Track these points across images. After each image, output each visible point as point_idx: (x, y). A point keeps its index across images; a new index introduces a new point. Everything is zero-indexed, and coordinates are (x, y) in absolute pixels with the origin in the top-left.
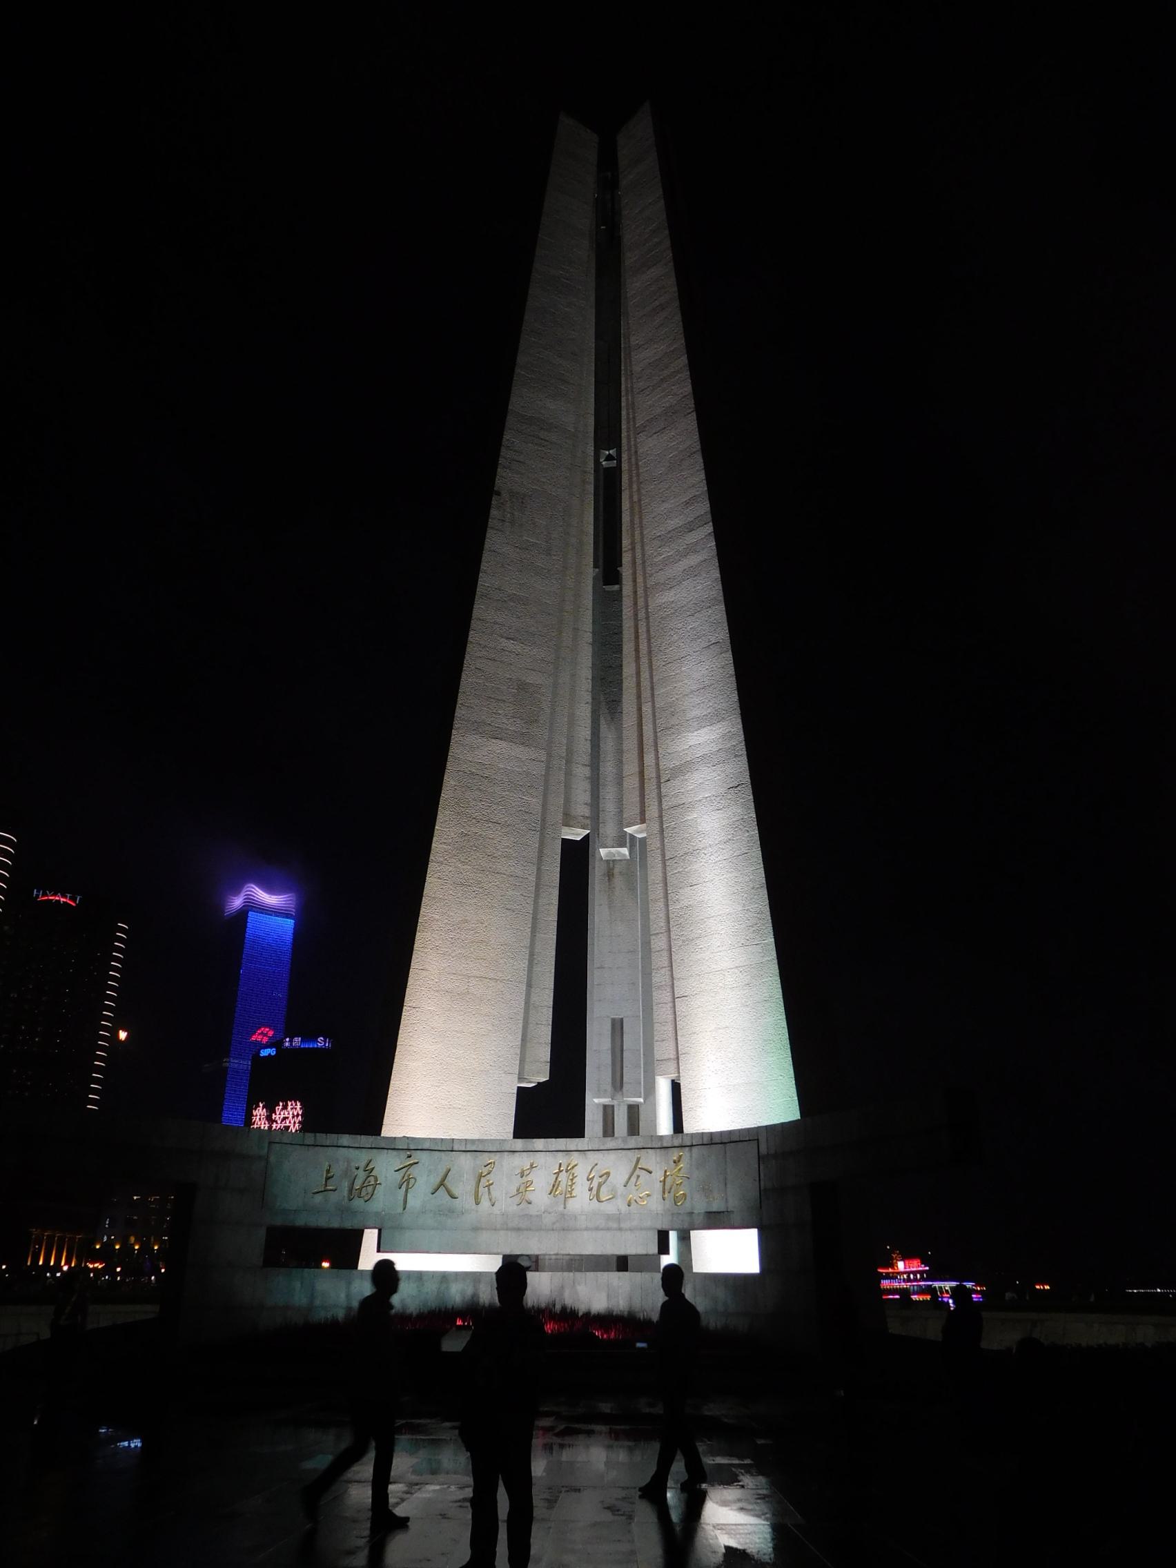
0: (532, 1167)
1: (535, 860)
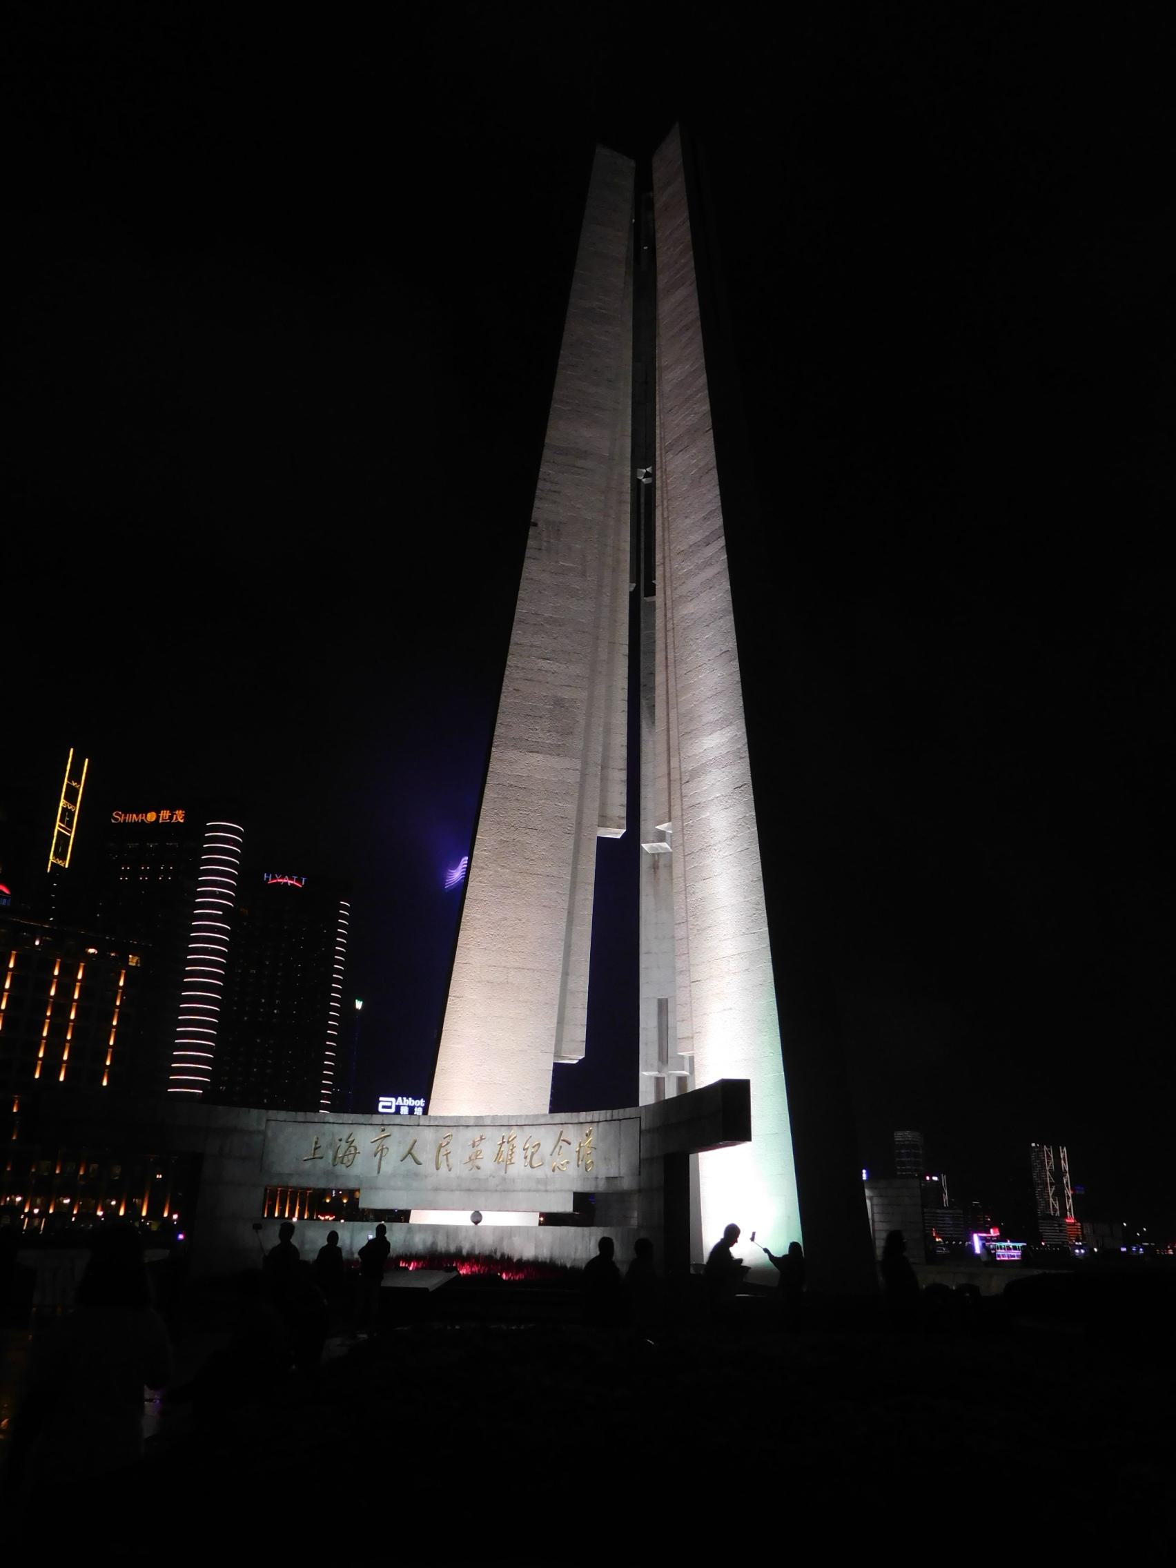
1: (570, 861)
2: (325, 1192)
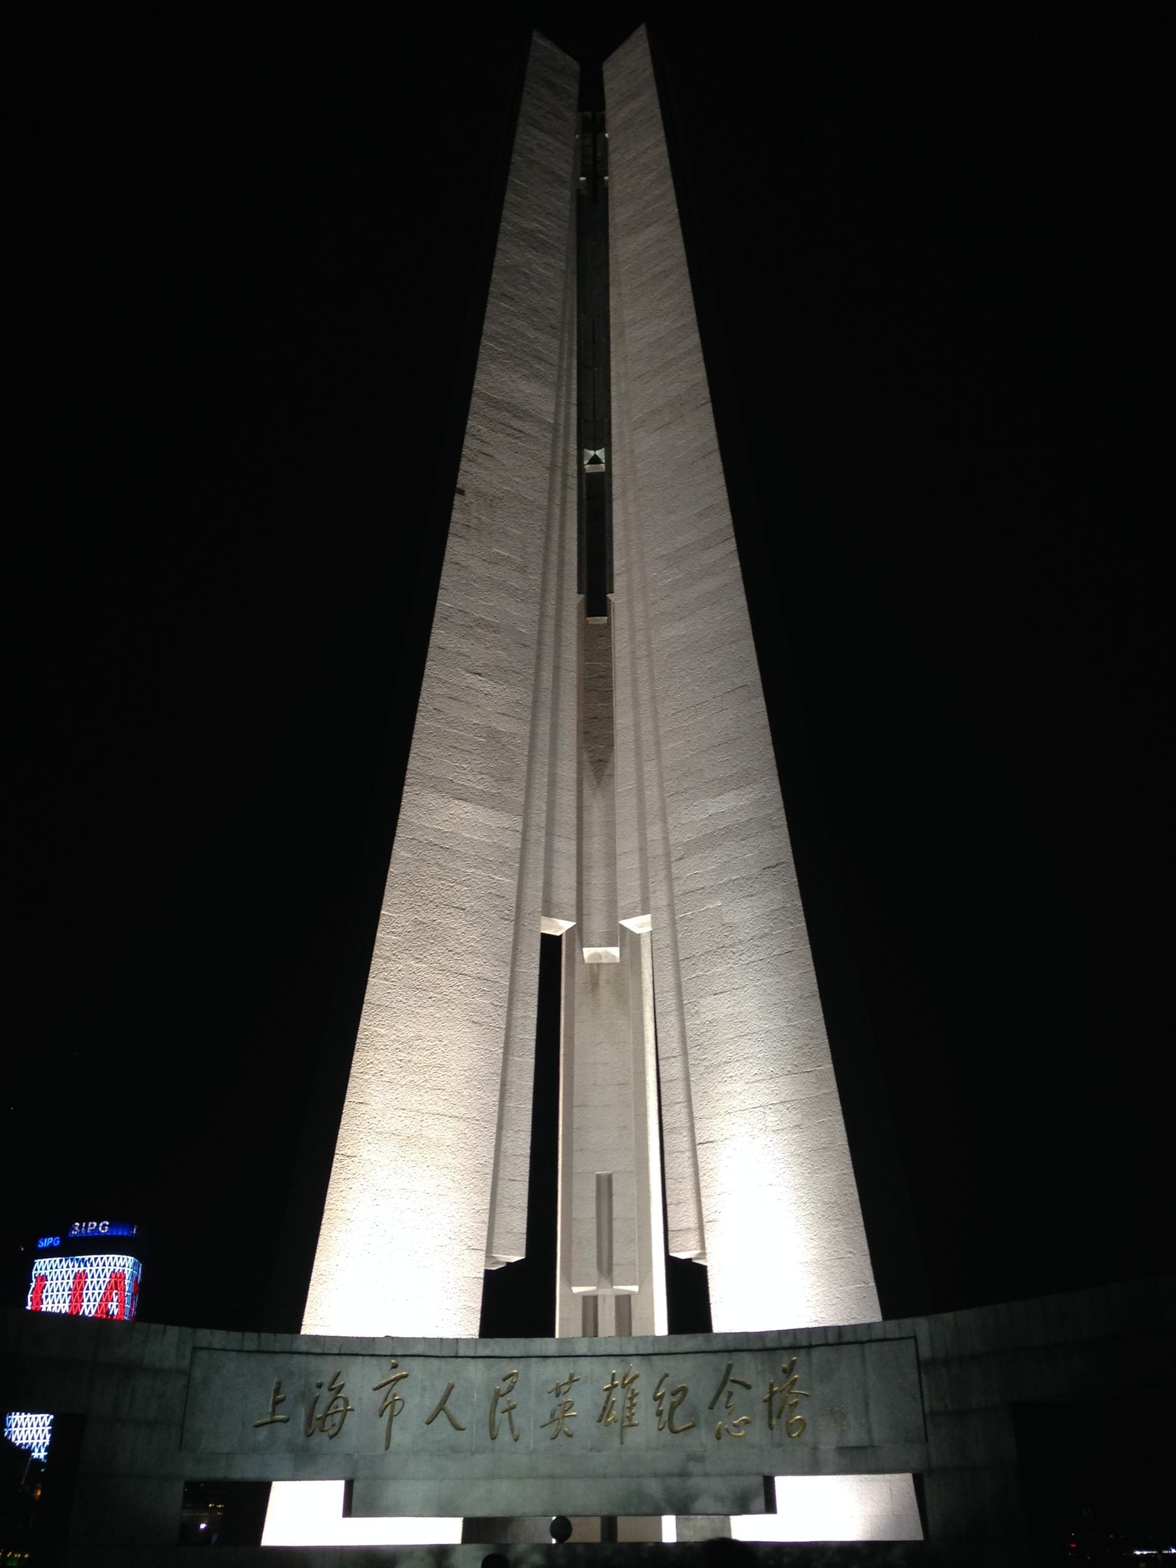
0: (572, 1380)
1: (508, 959)
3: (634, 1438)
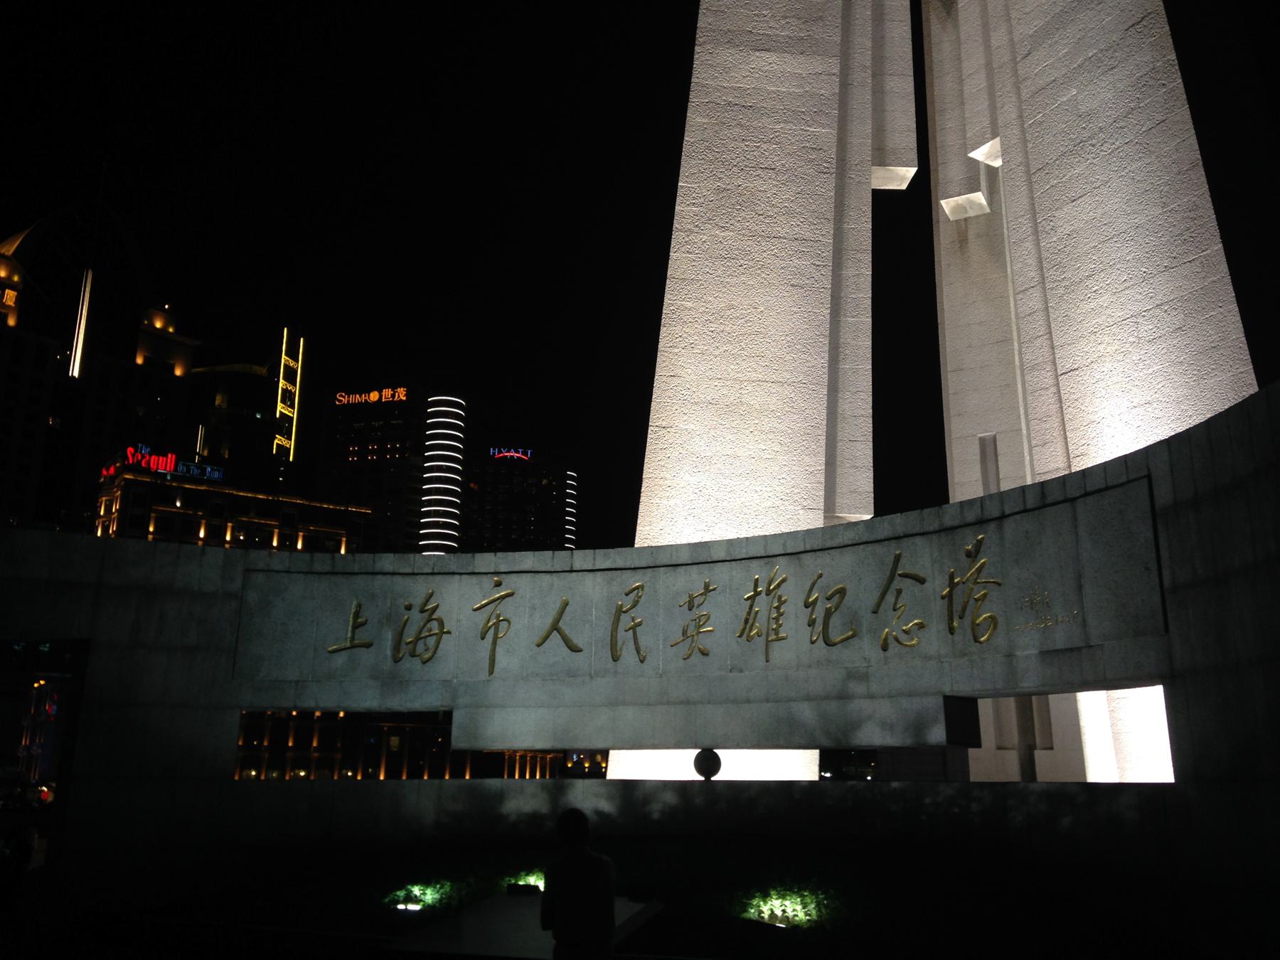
0: (707, 589)
1: (830, 215)
2: (565, 754)
3: (781, 653)
